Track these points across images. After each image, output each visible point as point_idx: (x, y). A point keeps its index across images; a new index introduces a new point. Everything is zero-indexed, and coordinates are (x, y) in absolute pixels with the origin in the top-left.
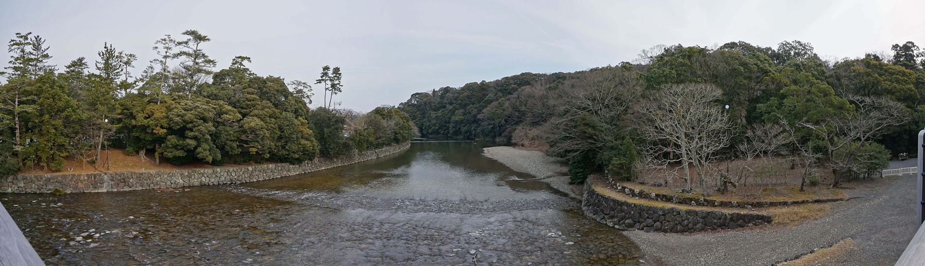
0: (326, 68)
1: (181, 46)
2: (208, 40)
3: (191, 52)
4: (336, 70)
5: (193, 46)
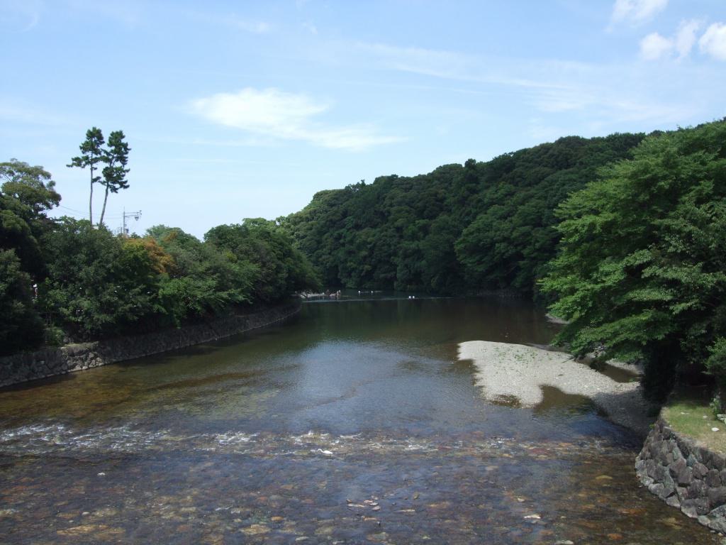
4: (117, 138)
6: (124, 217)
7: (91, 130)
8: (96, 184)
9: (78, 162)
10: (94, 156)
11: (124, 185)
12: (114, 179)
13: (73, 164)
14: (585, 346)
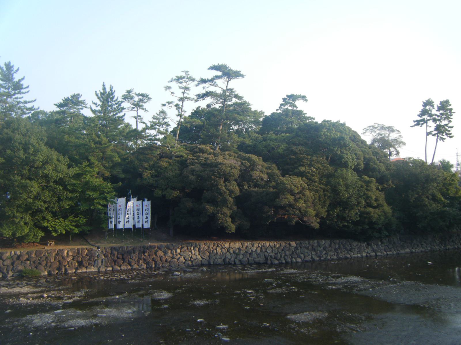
0: (429, 103)
1: (206, 85)
2: (243, 76)
3: (219, 91)
4: (445, 106)
5: (221, 85)
6: (457, 155)
7: (11, 65)
8: (430, 136)
9: (418, 123)
10: (429, 118)
11: (151, 99)
12: (442, 131)
13: (416, 125)
14: (49, 195)
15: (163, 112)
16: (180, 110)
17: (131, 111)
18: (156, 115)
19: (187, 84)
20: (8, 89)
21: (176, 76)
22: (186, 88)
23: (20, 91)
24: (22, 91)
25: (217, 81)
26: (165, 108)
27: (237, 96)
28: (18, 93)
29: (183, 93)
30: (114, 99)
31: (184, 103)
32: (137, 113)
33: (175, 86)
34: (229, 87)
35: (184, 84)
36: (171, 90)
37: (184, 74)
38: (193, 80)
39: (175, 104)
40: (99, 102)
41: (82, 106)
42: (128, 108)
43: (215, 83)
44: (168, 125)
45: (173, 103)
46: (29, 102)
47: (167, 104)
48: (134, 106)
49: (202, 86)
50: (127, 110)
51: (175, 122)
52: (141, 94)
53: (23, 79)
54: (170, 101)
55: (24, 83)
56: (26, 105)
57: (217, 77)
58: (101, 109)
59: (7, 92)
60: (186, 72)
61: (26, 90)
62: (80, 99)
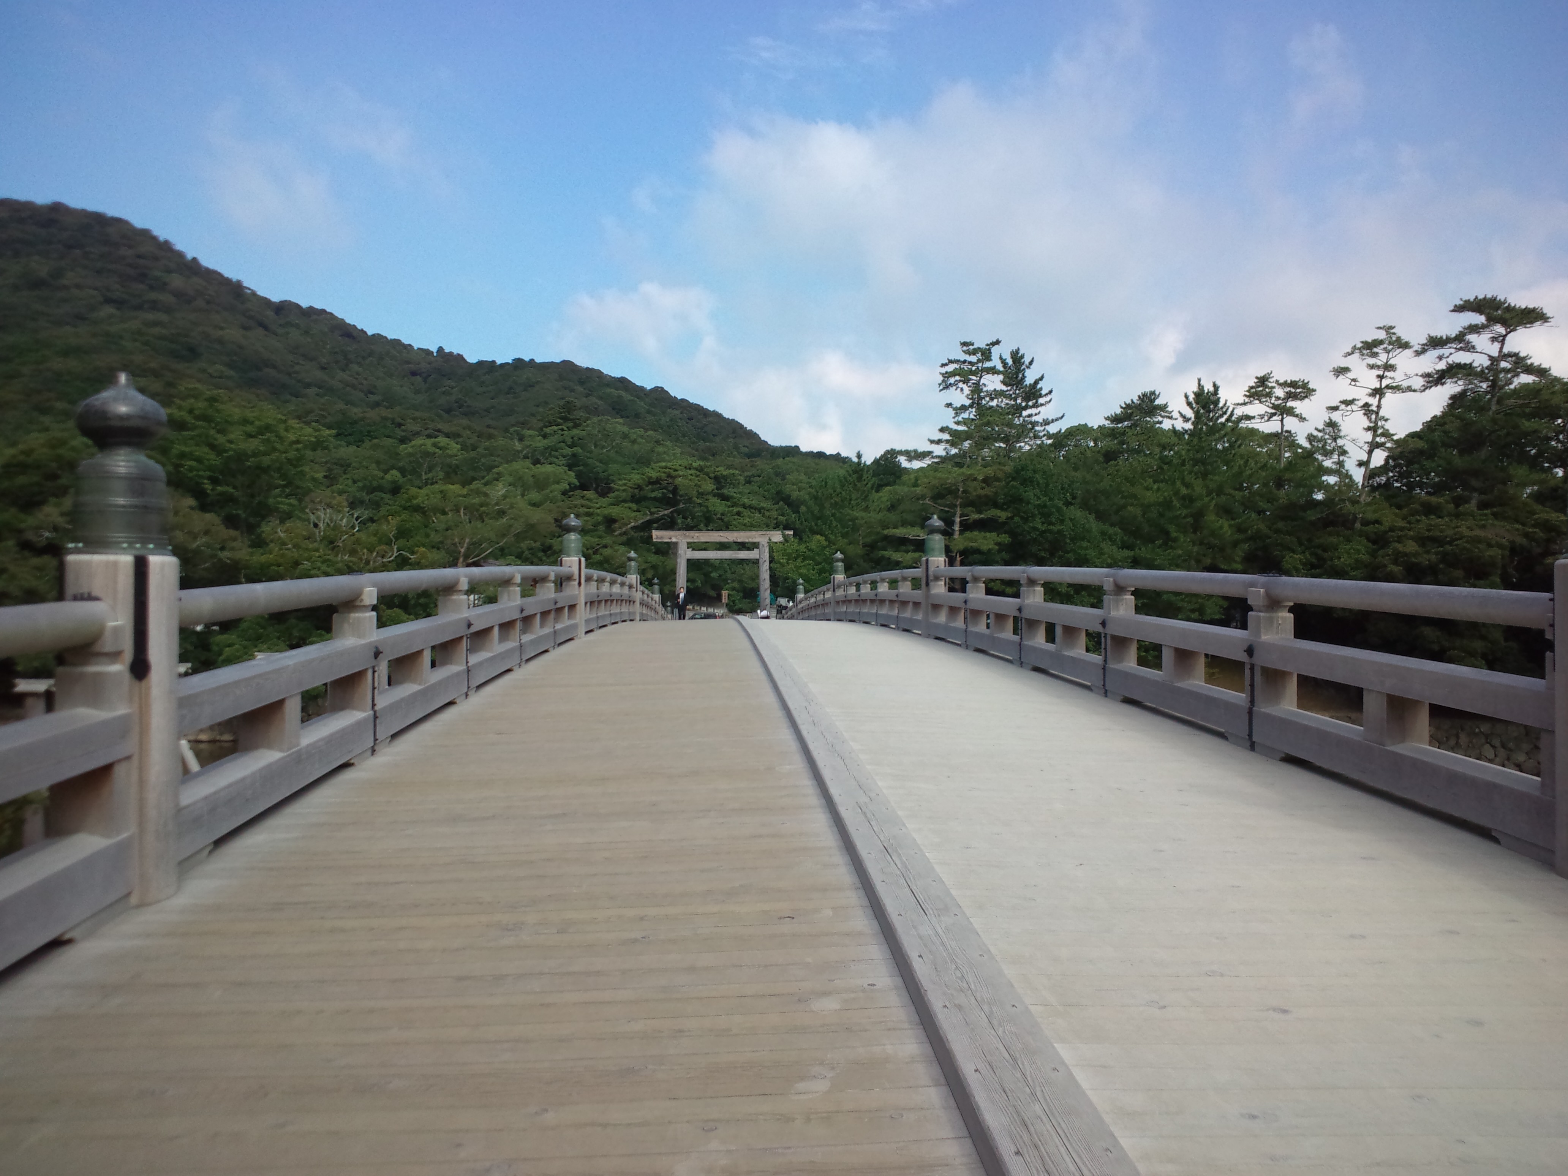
1: (1445, 351)
3: (1480, 361)
5: (1483, 350)
15: (1332, 424)
16: (1373, 417)
17: (1268, 420)
18: (1315, 433)
19: (1390, 356)
20: (1015, 399)
21: (1362, 342)
22: (1389, 367)
23: (1037, 402)
24: (1041, 401)
25: (1472, 338)
26: (1336, 416)
27: (1530, 370)
28: (1033, 406)
29: (1381, 377)
30: (1221, 405)
31: (1383, 401)
32: (1282, 425)
33: (1358, 365)
34: (1506, 350)
35: (1383, 358)
36: (1351, 375)
37: (1382, 335)
38: (1405, 346)
39: (1361, 403)
40: (1190, 414)
41: (1162, 417)
42: (1262, 417)
43: (1469, 342)
44: (1344, 453)
45: (1356, 402)
46: (1053, 421)
47: (1343, 407)
48: (1273, 411)
49: (1433, 354)
50: (1259, 421)
51: (1361, 444)
52: (1289, 381)
53: (1041, 378)
54: (1350, 398)
55: (1044, 387)
56: (1047, 427)
57: (1474, 329)
58: (1192, 427)
59: (1013, 405)
60: (1389, 329)
61: (1048, 398)
62: (1158, 402)
